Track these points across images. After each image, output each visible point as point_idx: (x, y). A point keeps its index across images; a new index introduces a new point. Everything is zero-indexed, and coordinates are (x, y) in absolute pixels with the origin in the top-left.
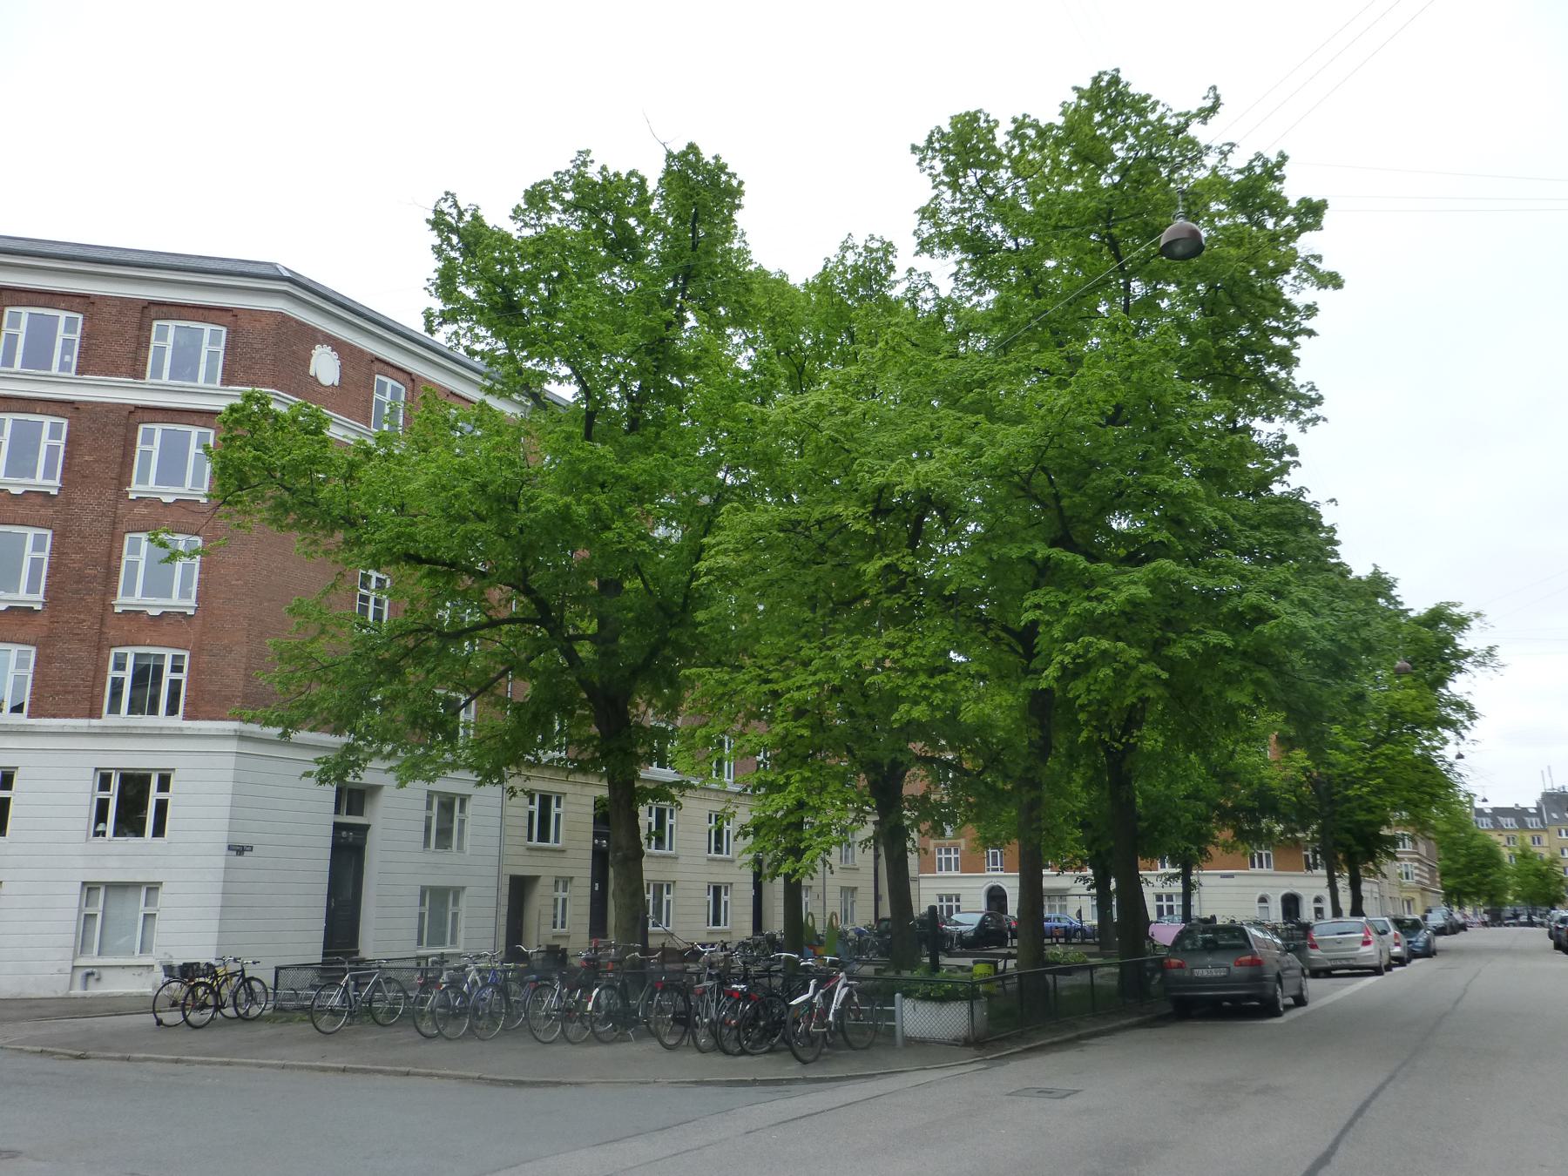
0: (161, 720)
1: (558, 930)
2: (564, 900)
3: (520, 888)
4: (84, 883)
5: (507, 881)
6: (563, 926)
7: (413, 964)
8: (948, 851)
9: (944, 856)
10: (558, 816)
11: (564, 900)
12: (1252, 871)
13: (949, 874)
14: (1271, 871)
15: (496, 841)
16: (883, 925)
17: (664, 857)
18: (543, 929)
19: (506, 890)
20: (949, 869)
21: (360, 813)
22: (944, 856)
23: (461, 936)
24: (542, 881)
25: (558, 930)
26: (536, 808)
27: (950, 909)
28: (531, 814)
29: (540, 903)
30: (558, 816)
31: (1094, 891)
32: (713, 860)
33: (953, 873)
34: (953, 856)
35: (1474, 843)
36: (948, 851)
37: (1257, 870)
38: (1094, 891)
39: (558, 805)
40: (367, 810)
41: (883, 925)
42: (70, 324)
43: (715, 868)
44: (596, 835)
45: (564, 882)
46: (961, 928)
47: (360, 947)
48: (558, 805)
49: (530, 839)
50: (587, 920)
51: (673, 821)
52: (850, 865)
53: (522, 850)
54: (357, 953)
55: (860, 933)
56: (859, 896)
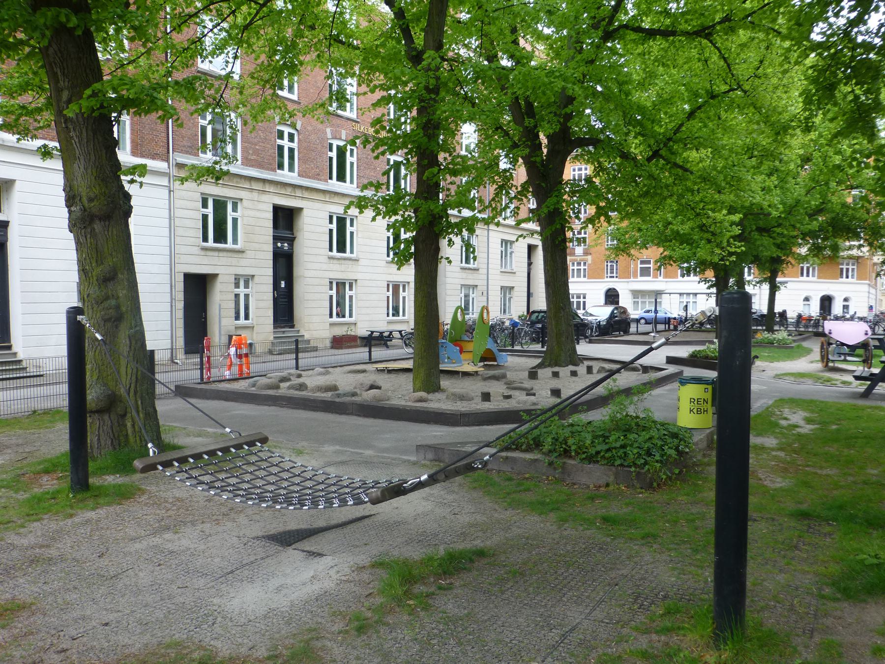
1: (242, 321)
2: (247, 296)
5: (181, 278)
6: (247, 317)
8: (579, 264)
9: (576, 267)
10: (235, 221)
11: (247, 296)
12: (801, 279)
14: (815, 279)
15: (166, 242)
16: (534, 317)
17: (345, 259)
18: (225, 322)
19: (180, 286)
20: (579, 276)
22: (576, 267)
25: (242, 321)
26: (334, 226)
27: (578, 303)
28: (331, 231)
29: (220, 301)
30: (235, 221)
31: (714, 290)
33: (582, 279)
34: (582, 267)
36: (579, 264)
37: (805, 278)
38: (714, 290)
39: (352, 225)
41: (534, 317)
43: (335, 266)
44: (276, 239)
46: (590, 318)
47: (13, 342)
48: (352, 225)
49: (331, 250)
50: (270, 313)
51: (352, 229)
52: (508, 269)
55: (514, 324)
56: (515, 293)
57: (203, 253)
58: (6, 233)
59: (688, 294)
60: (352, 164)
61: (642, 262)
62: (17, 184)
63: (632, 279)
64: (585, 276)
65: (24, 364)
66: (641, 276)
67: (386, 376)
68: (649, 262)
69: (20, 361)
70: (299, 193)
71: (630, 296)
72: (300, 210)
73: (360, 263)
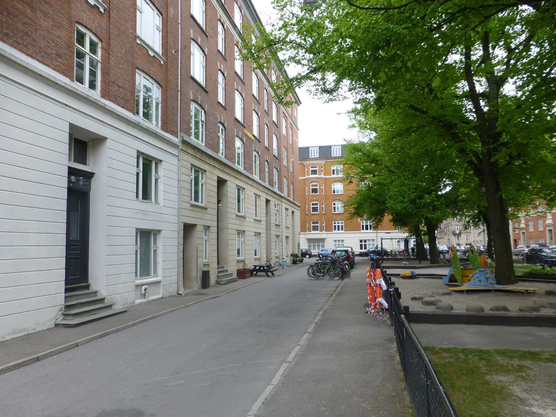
0: (369, 231)
2: (365, 245)
3: (188, 229)
4: (137, 229)
7: (259, 273)
13: (339, 232)
18: (199, 260)
20: (339, 230)
21: (84, 163)
22: (337, 225)
23: (160, 267)
24: (198, 226)
32: (192, 206)
33: (340, 231)
35: (386, 160)
40: (90, 160)
42: (312, 156)
45: (207, 228)
47: (90, 281)
51: (203, 181)
53: (188, 206)
54: (88, 287)
57: (191, 208)
58: (90, 183)
59: (339, 241)
60: (238, 154)
61: (313, 223)
62: (108, 140)
63: (308, 232)
64: (371, 229)
65: (107, 302)
66: (313, 230)
67: (460, 297)
68: (317, 223)
69: (102, 300)
70: (226, 170)
71: (306, 242)
72: (226, 181)
73: (247, 219)
